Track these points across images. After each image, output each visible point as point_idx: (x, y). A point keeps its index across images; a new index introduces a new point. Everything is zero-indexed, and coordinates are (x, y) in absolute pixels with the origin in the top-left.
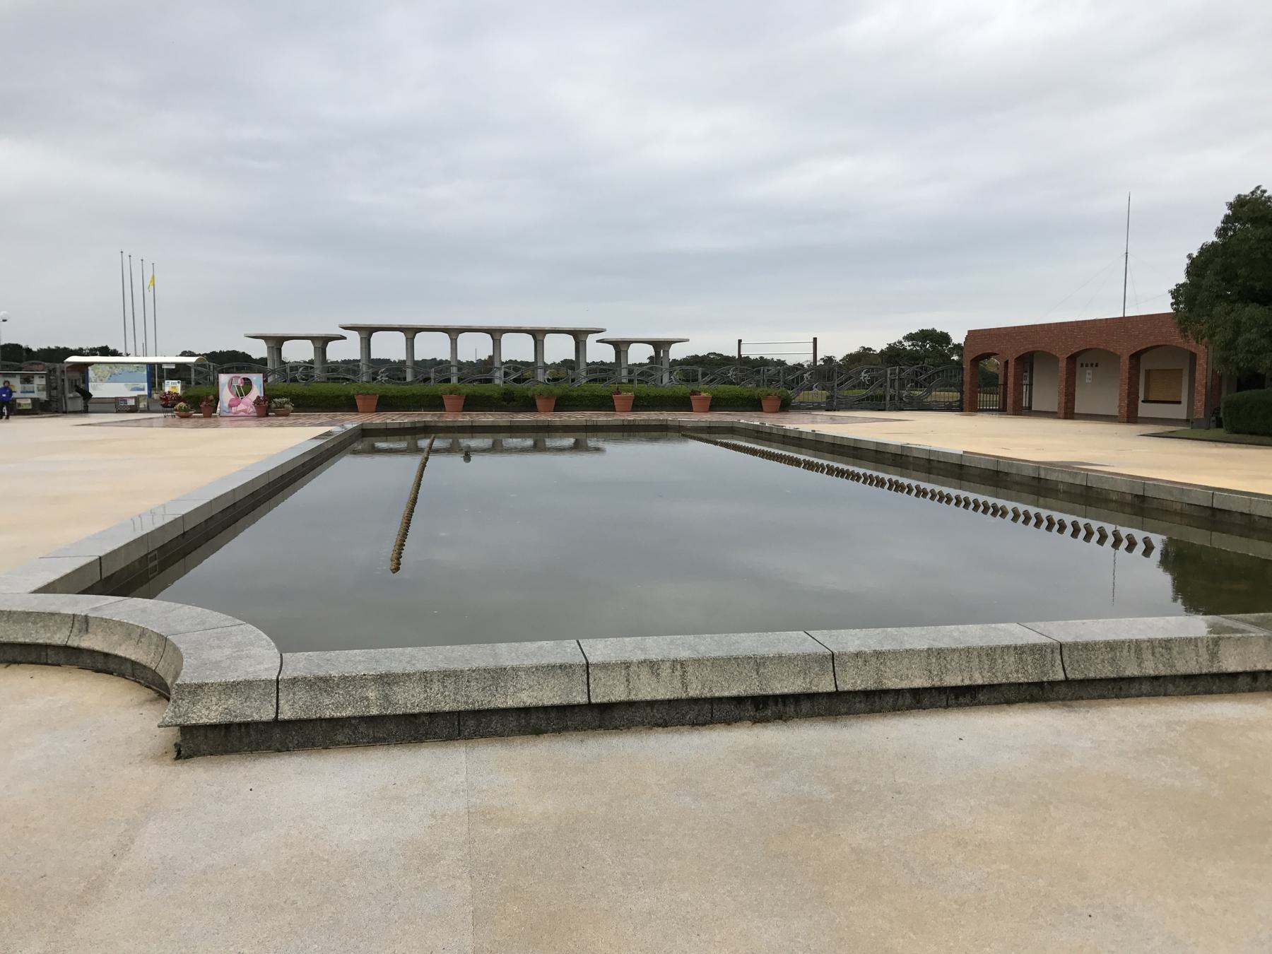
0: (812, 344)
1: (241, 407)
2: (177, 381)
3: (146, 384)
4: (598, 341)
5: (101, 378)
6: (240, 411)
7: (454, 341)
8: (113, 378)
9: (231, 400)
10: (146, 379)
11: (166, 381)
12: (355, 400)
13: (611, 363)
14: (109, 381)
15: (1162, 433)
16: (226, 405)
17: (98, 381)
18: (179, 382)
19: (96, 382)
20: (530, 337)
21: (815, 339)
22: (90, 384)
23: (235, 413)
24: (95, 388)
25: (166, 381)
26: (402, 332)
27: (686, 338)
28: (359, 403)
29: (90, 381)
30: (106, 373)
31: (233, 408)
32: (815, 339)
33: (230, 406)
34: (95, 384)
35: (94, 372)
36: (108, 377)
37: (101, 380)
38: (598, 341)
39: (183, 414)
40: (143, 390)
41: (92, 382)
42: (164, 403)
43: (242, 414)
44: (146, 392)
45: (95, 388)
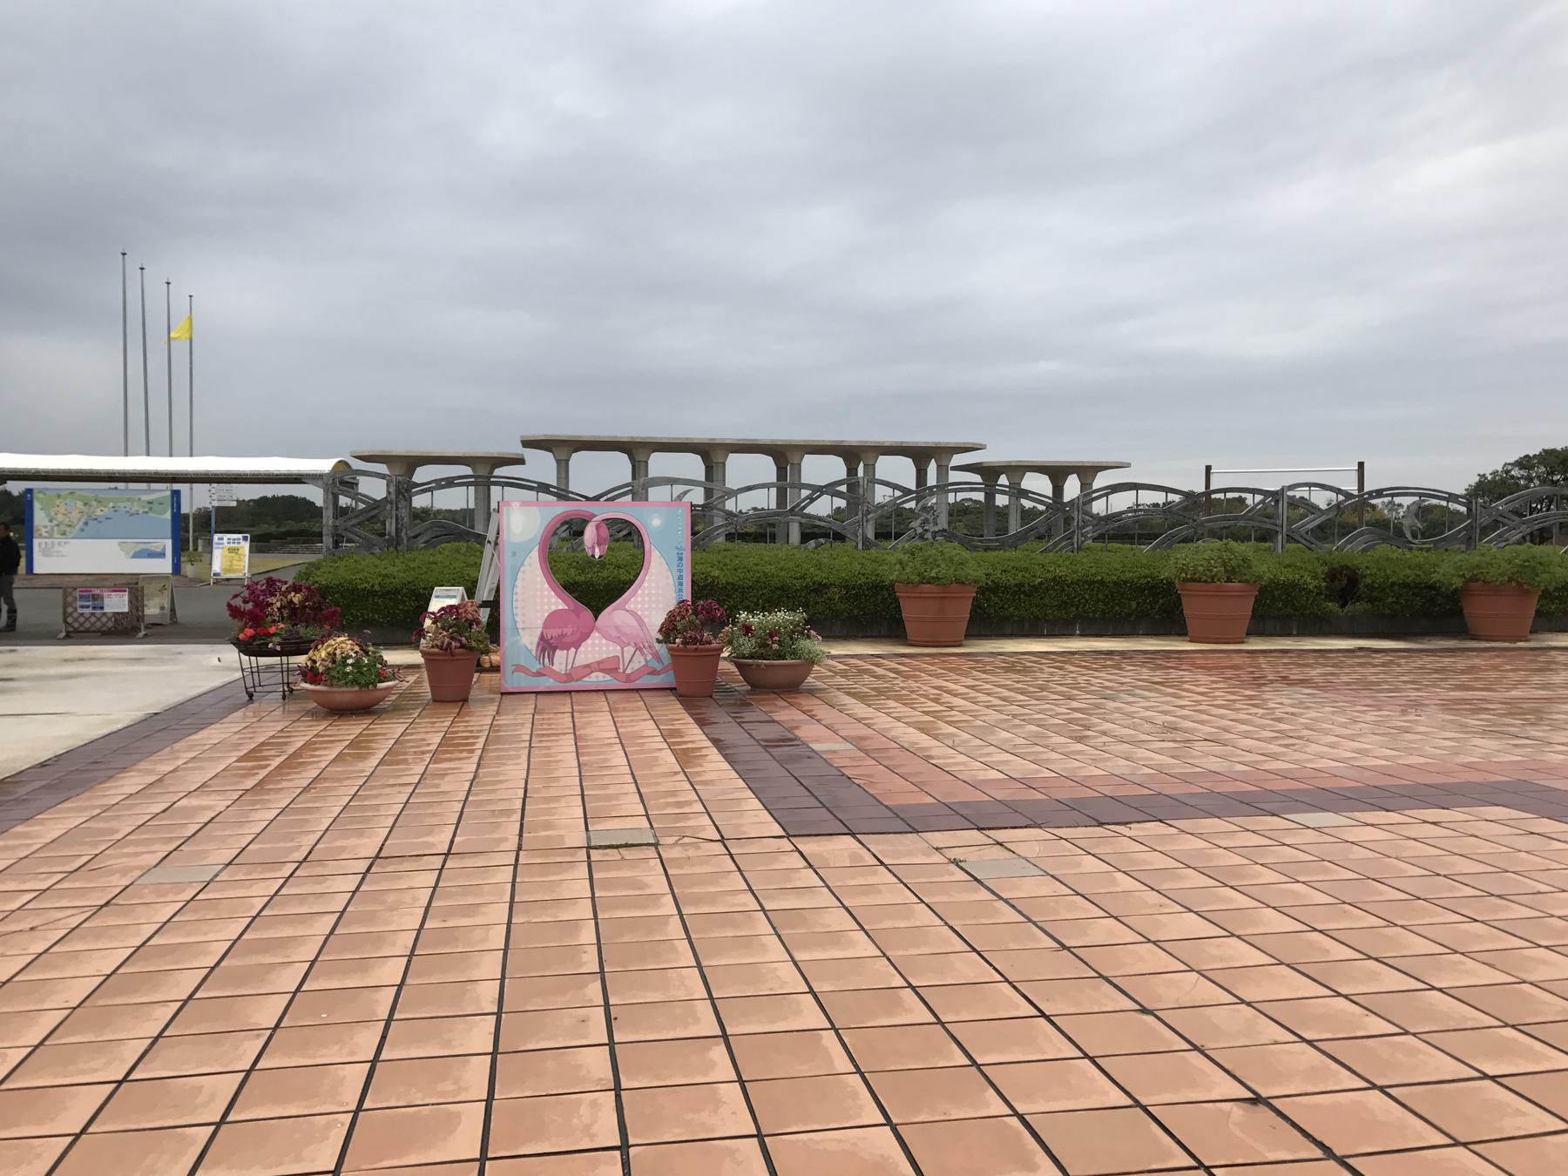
0: (195, 486)
1: (595, 648)
2: (240, 536)
3: (169, 544)
4: (1128, 465)
5: (63, 528)
6: (590, 669)
7: (563, 463)
8: (91, 528)
9: (553, 619)
10: (169, 534)
11: (216, 537)
12: (897, 600)
13: (461, 510)
14: (83, 534)
15: (736, 895)
16: (529, 640)
17: (56, 535)
18: (245, 539)
19: (51, 537)
20: (769, 460)
21: (1361, 465)
22: (36, 542)
23: (569, 677)
24: (46, 553)
25: (216, 537)
26: (550, 451)
27: (1126, 461)
28: (910, 611)
29: (35, 534)
30: (75, 515)
31: (560, 655)
32: (1361, 465)
33: (548, 646)
34: (49, 541)
35: (48, 515)
36: (80, 525)
37: (64, 534)
38: (1128, 465)
39: (346, 694)
40: (162, 555)
41: (41, 536)
42: (250, 632)
43: (598, 679)
44: (164, 566)
45: (46, 553)
